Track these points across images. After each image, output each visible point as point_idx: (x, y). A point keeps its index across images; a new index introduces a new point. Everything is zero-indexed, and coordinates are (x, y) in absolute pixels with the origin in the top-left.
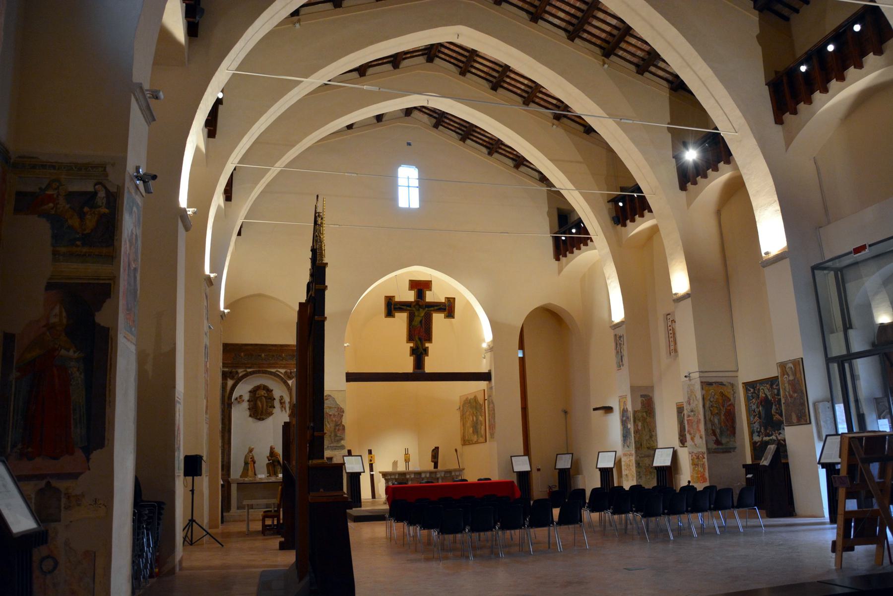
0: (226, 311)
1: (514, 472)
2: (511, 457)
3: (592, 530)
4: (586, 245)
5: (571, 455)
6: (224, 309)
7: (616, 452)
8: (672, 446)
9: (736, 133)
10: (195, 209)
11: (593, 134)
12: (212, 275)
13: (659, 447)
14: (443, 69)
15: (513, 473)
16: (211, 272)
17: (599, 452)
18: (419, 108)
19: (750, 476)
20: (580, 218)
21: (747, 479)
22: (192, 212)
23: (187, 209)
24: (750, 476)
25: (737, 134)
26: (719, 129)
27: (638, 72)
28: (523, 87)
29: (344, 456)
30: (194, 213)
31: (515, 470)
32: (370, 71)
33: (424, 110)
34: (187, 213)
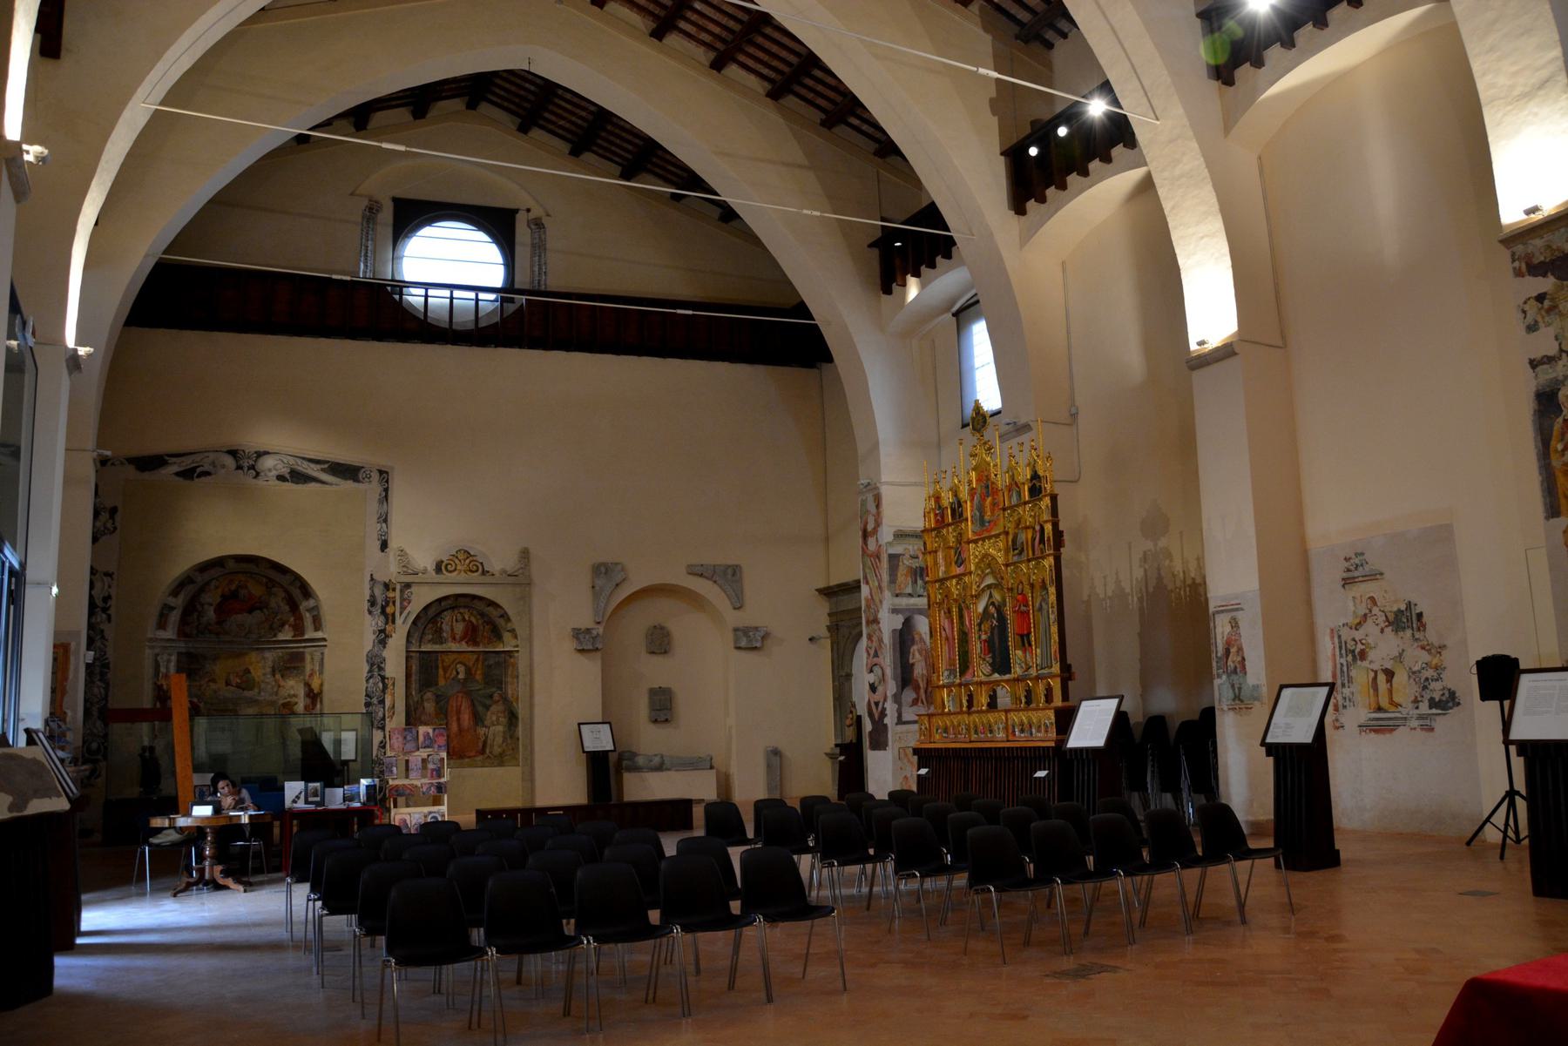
0: (82, 351)
1: (584, 752)
2: (579, 724)
3: (837, 892)
4: (948, 256)
5: (581, 726)
6: (76, 345)
7: (579, 724)
8: (607, 721)
9: (1157, 119)
10: (92, 350)
11: (734, 223)
12: (82, 351)
13: (360, 715)
14: (494, 122)
15: (582, 754)
16: (79, 342)
17: (609, 723)
18: (505, 75)
19: (923, 771)
20: (933, 203)
21: (919, 776)
22: (37, 157)
23: (25, 147)
24: (923, 771)
25: (1158, 123)
26: (1124, 107)
27: (823, 123)
28: (717, 30)
29: (1121, 698)
30: (41, 159)
31: (586, 750)
32: (379, 118)
33: (513, 79)
34: (22, 155)
